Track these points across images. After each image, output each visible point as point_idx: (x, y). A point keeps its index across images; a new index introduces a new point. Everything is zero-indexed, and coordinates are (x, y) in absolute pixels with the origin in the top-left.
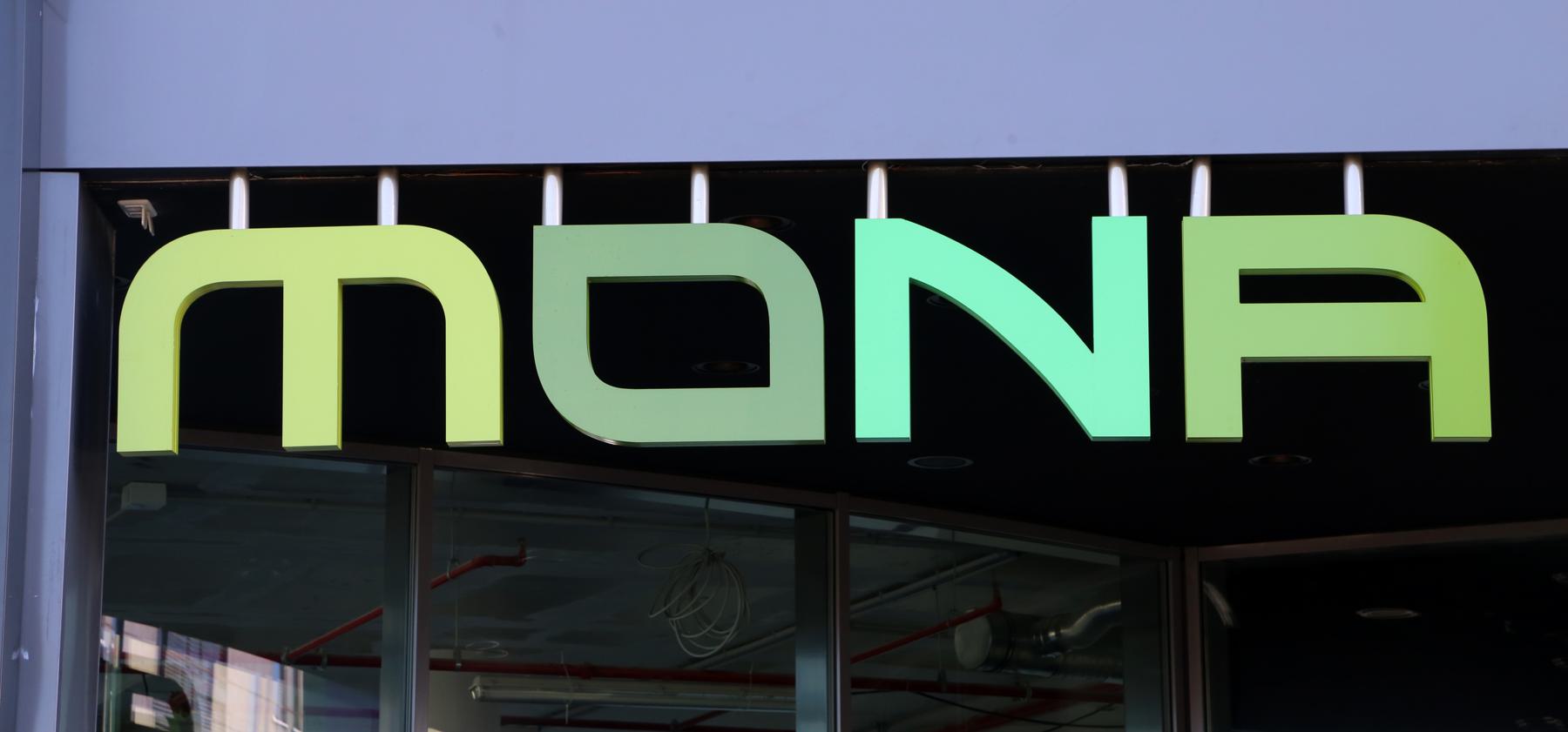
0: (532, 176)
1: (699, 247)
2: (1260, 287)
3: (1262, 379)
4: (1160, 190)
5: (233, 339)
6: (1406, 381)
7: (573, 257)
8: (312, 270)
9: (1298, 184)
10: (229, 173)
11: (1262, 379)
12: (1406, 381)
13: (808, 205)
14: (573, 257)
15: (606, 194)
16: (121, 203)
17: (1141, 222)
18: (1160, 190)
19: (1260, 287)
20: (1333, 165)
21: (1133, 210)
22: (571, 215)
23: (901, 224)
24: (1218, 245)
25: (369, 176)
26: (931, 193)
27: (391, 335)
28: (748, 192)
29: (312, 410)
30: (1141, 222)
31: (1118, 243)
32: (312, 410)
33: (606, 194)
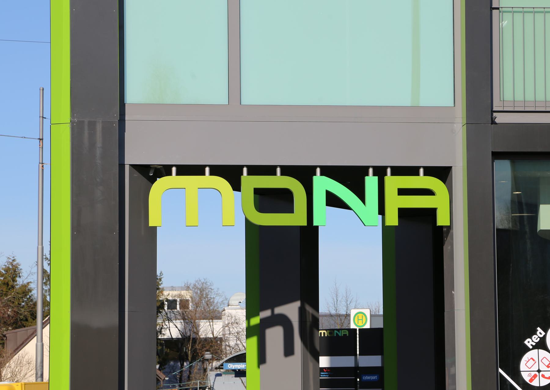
0: (242, 167)
1: (278, 181)
2: (402, 192)
3: (403, 213)
4: (380, 172)
5: (321, 333)
6: (432, 213)
7: (251, 183)
8: (322, 332)
9: (413, 171)
10: (242, 167)
11: (403, 213)
12: (432, 213)
13: (304, 175)
14: (251, 183)
15: (255, 170)
16: (539, 329)
17: (376, 178)
18: (380, 172)
19: (402, 192)
20: (275, 167)
21: (374, 175)
22: (249, 174)
23: (324, 178)
24: (393, 183)
25: (419, 168)
26: (330, 172)
27: (324, 333)
28: (287, 171)
29: (322, 335)
30: (376, 178)
31: (371, 183)
32: (322, 335)
33: (255, 170)
